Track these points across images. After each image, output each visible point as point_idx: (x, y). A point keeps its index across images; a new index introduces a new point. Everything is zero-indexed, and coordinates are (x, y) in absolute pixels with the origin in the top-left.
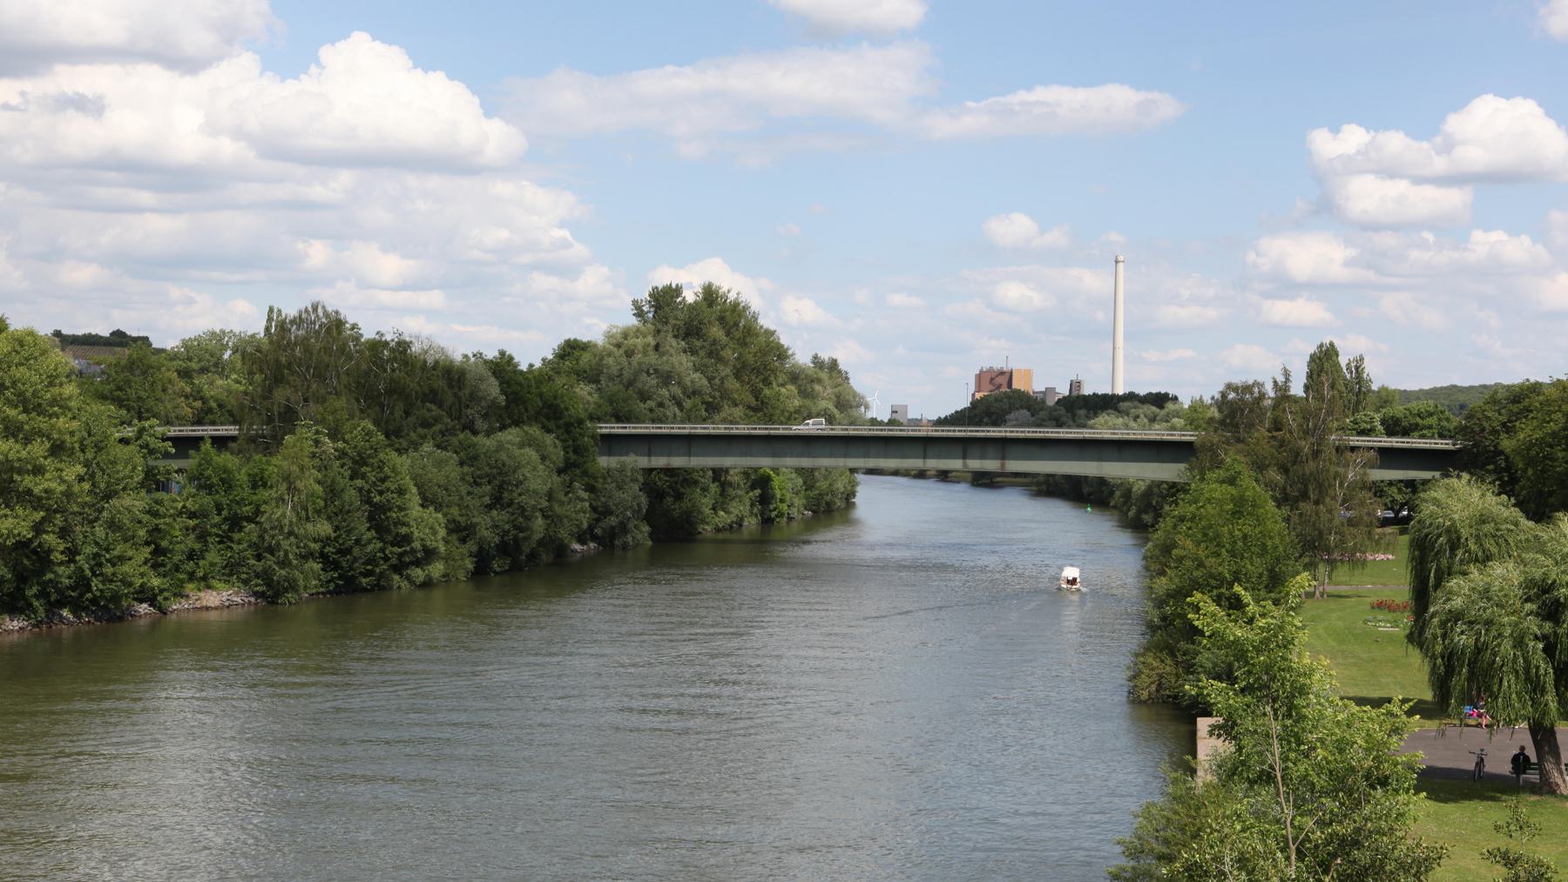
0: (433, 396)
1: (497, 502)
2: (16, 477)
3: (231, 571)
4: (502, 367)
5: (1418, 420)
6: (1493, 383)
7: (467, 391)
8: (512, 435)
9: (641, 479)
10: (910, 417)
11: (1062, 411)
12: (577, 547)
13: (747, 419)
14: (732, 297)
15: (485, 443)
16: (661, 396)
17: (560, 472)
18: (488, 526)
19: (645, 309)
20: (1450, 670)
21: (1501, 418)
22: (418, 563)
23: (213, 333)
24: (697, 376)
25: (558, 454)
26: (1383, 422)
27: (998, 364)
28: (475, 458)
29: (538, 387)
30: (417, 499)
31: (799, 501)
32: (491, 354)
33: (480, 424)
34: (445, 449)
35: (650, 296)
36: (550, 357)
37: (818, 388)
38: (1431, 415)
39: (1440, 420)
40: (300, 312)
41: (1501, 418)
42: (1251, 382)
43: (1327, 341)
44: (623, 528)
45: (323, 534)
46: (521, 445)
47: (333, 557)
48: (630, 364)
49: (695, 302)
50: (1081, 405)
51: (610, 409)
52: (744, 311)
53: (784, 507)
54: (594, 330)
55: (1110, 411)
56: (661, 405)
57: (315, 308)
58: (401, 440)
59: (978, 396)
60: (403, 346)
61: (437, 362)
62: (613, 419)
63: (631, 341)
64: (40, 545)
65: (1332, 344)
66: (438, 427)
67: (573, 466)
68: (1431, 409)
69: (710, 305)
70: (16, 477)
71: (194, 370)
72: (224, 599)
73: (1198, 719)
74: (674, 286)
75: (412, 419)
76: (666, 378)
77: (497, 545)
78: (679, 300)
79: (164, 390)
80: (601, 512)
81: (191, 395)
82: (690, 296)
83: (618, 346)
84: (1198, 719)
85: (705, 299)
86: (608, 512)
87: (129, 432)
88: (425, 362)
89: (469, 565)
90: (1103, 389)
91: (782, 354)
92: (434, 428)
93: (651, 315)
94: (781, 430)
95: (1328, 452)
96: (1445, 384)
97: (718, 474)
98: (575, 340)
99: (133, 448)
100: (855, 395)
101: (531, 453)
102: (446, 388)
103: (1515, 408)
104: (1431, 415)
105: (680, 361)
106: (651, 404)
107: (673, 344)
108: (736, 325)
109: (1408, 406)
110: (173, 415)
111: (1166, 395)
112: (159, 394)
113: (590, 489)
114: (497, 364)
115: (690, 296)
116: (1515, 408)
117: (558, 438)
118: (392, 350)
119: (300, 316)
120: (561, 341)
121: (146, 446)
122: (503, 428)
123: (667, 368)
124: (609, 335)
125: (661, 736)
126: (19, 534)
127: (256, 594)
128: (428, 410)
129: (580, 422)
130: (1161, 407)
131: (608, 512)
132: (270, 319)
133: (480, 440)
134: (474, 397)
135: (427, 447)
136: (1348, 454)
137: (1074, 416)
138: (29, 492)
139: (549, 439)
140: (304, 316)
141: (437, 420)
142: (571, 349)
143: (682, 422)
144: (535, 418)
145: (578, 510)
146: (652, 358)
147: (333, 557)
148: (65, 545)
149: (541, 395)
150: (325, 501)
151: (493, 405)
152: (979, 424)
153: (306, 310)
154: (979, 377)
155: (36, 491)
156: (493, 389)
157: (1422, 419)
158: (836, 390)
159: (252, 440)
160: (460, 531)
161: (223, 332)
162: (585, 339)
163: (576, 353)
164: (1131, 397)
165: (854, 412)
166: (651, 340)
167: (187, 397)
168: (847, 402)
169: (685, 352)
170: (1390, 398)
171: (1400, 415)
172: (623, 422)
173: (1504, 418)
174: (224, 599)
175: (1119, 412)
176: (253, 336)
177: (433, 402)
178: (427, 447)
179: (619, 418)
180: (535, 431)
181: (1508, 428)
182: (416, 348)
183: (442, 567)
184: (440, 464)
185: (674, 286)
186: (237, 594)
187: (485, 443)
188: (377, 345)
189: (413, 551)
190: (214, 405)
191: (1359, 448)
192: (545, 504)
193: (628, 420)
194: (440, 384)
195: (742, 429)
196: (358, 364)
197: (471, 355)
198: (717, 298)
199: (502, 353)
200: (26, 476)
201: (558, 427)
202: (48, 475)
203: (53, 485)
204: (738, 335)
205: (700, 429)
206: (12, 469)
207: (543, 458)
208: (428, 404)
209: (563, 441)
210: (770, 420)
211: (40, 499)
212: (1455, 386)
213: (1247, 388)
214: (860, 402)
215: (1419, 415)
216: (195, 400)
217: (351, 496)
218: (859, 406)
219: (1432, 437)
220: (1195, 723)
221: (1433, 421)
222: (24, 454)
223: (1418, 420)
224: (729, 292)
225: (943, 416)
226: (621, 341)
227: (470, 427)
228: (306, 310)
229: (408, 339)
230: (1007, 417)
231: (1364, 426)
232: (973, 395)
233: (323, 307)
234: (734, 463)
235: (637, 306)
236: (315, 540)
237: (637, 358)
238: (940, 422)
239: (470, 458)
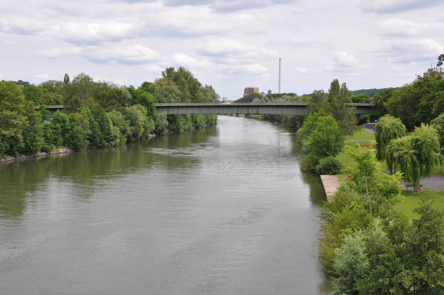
0: (114, 97)
1: (132, 125)
2: (9, 120)
3: (65, 144)
4: (131, 90)
5: (361, 99)
6: (373, 89)
7: (122, 96)
8: (134, 107)
9: (166, 118)
10: (228, 100)
11: (267, 98)
12: (151, 135)
13: (191, 102)
14: (187, 70)
15: (128, 109)
16: (170, 96)
17: (147, 116)
18: (130, 130)
19: (165, 74)
20: (415, 166)
21: (383, 98)
22: (113, 140)
23: (50, 81)
24: (179, 91)
25: (146, 111)
26: (352, 99)
27: (250, 86)
28: (126, 113)
29: (140, 95)
30: (112, 124)
31: (204, 122)
32: (128, 86)
33: (126, 104)
34: (118, 111)
35: (166, 70)
36: (140, 86)
37: (208, 93)
38: (364, 97)
39: (366, 98)
40: (78, 76)
41: (383, 98)
42: (320, 90)
43: (336, 79)
44: (163, 130)
45: (89, 134)
46: (137, 109)
47: (91, 139)
48: (162, 88)
49: (177, 72)
50: (270, 96)
51: (157, 100)
52: (190, 74)
53: (201, 124)
54: (152, 80)
55: (280, 98)
56: (170, 98)
57: (82, 75)
58: (106, 109)
59: (246, 94)
60: (105, 84)
61: (114, 88)
62: (158, 102)
63: (162, 83)
64: (17, 137)
65: (337, 80)
66: (116, 105)
67: (150, 114)
68: (364, 96)
69: (181, 72)
70: (9, 120)
71: (47, 91)
72: (64, 150)
73: (321, 175)
74: (172, 68)
75: (108, 103)
76: (171, 92)
77: (132, 135)
78: (173, 71)
79: (39, 96)
80: (157, 126)
81: (47, 97)
82: (176, 70)
83: (159, 84)
84: (321, 175)
85: (180, 71)
86: (158, 126)
87: (38, 107)
88: (111, 89)
89: (126, 140)
90: (277, 92)
91: (199, 84)
92: (115, 105)
93: (166, 75)
94: (201, 104)
95: (344, 107)
96: (361, 89)
97: (184, 115)
98: (147, 82)
99: (40, 112)
100: (217, 95)
101: (140, 111)
102: (117, 95)
103: (386, 95)
104: (364, 97)
105: (175, 87)
106: (167, 98)
107: (172, 83)
108: (188, 77)
109: (358, 95)
110: (42, 102)
111: (293, 94)
112: (38, 97)
113: (155, 120)
114: (130, 89)
115: (176, 70)
116: (386, 95)
117: (146, 107)
118: (103, 85)
119: (78, 77)
120: (143, 82)
121: (43, 111)
122: (132, 105)
123: (171, 89)
124: (156, 81)
125: (147, 173)
126: (11, 135)
127: (72, 149)
128: (113, 101)
129: (151, 103)
130: (293, 97)
131: (158, 126)
132: (65, 77)
133: (127, 108)
134: (124, 98)
135: (114, 110)
136: (349, 108)
137: (270, 99)
138: (13, 124)
139: (143, 108)
140: (79, 77)
141: (115, 104)
142: (146, 85)
143: (176, 103)
144: (140, 103)
145: (152, 125)
146: (167, 86)
147: (91, 139)
148: (23, 138)
149: (141, 97)
150: (89, 125)
151: (130, 99)
152: (246, 102)
153: (80, 75)
154: (245, 90)
155: (15, 123)
156: (129, 96)
157: (362, 98)
158: (212, 94)
159: (67, 109)
160: (123, 132)
161: (53, 81)
162: (149, 82)
163: (147, 85)
164: (284, 94)
165: (216, 99)
166: (167, 82)
167: (45, 98)
168: (215, 97)
169: (176, 85)
170: (351, 93)
171: (356, 97)
172: (160, 103)
173: (383, 98)
174: (64, 150)
175: (282, 98)
176: (61, 82)
177: (114, 98)
178: (114, 110)
179: (159, 102)
180: (140, 106)
181: (385, 100)
182: (108, 85)
183: (119, 141)
184: (117, 115)
185: (172, 68)
186: (67, 149)
187: (128, 109)
188: (99, 84)
189: (112, 137)
190: (52, 100)
191: (351, 106)
192: (144, 123)
193: (162, 103)
194: (116, 94)
195: (190, 104)
196: (94, 89)
197: (123, 86)
198: (183, 70)
199: (131, 86)
200: (12, 119)
201: (146, 105)
202: (18, 119)
203: (19, 122)
204: (188, 80)
205: (181, 104)
206: (8, 118)
207: (142, 112)
208: (113, 99)
209: (147, 108)
210: (197, 102)
211: (15, 125)
212: (364, 90)
213: (319, 91)
214: (217, 96)
215: (361, 97)
216: (48, 98)
217: (96, 123)
218: (217, 98)
219: (364, 103)
220: (320, 177)
221: (364, 99)
222: (11, 114)
223: (361, 99)
224: (186, 69)
225: (236, 100)
226: (159, 82)
227: (123, 105)
228: (80, 75)
229: (106, 82)
230: (253, 100)
231: (347, 100)
232: (244, 94)
233: (84, 74)
234: (188, 112)
235: (163, 73)
236: (87, 135)
237: (163, 87)
238: (235, 102)
239: (125, 113)
